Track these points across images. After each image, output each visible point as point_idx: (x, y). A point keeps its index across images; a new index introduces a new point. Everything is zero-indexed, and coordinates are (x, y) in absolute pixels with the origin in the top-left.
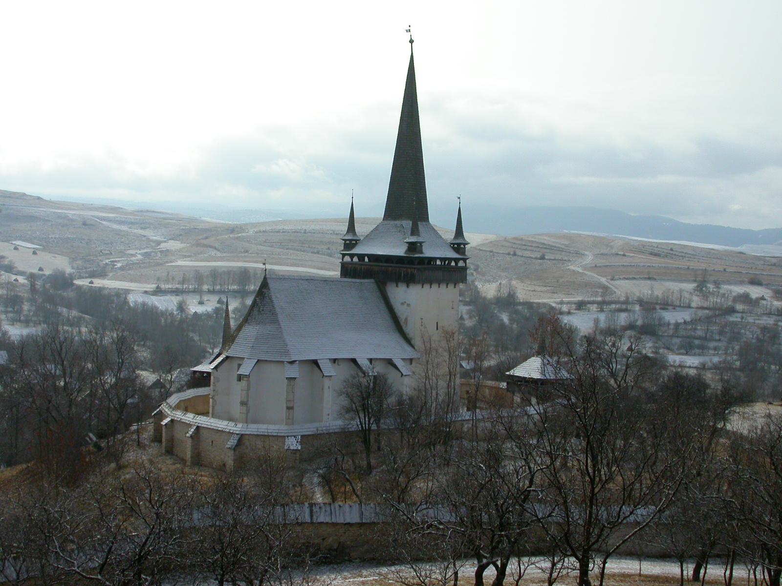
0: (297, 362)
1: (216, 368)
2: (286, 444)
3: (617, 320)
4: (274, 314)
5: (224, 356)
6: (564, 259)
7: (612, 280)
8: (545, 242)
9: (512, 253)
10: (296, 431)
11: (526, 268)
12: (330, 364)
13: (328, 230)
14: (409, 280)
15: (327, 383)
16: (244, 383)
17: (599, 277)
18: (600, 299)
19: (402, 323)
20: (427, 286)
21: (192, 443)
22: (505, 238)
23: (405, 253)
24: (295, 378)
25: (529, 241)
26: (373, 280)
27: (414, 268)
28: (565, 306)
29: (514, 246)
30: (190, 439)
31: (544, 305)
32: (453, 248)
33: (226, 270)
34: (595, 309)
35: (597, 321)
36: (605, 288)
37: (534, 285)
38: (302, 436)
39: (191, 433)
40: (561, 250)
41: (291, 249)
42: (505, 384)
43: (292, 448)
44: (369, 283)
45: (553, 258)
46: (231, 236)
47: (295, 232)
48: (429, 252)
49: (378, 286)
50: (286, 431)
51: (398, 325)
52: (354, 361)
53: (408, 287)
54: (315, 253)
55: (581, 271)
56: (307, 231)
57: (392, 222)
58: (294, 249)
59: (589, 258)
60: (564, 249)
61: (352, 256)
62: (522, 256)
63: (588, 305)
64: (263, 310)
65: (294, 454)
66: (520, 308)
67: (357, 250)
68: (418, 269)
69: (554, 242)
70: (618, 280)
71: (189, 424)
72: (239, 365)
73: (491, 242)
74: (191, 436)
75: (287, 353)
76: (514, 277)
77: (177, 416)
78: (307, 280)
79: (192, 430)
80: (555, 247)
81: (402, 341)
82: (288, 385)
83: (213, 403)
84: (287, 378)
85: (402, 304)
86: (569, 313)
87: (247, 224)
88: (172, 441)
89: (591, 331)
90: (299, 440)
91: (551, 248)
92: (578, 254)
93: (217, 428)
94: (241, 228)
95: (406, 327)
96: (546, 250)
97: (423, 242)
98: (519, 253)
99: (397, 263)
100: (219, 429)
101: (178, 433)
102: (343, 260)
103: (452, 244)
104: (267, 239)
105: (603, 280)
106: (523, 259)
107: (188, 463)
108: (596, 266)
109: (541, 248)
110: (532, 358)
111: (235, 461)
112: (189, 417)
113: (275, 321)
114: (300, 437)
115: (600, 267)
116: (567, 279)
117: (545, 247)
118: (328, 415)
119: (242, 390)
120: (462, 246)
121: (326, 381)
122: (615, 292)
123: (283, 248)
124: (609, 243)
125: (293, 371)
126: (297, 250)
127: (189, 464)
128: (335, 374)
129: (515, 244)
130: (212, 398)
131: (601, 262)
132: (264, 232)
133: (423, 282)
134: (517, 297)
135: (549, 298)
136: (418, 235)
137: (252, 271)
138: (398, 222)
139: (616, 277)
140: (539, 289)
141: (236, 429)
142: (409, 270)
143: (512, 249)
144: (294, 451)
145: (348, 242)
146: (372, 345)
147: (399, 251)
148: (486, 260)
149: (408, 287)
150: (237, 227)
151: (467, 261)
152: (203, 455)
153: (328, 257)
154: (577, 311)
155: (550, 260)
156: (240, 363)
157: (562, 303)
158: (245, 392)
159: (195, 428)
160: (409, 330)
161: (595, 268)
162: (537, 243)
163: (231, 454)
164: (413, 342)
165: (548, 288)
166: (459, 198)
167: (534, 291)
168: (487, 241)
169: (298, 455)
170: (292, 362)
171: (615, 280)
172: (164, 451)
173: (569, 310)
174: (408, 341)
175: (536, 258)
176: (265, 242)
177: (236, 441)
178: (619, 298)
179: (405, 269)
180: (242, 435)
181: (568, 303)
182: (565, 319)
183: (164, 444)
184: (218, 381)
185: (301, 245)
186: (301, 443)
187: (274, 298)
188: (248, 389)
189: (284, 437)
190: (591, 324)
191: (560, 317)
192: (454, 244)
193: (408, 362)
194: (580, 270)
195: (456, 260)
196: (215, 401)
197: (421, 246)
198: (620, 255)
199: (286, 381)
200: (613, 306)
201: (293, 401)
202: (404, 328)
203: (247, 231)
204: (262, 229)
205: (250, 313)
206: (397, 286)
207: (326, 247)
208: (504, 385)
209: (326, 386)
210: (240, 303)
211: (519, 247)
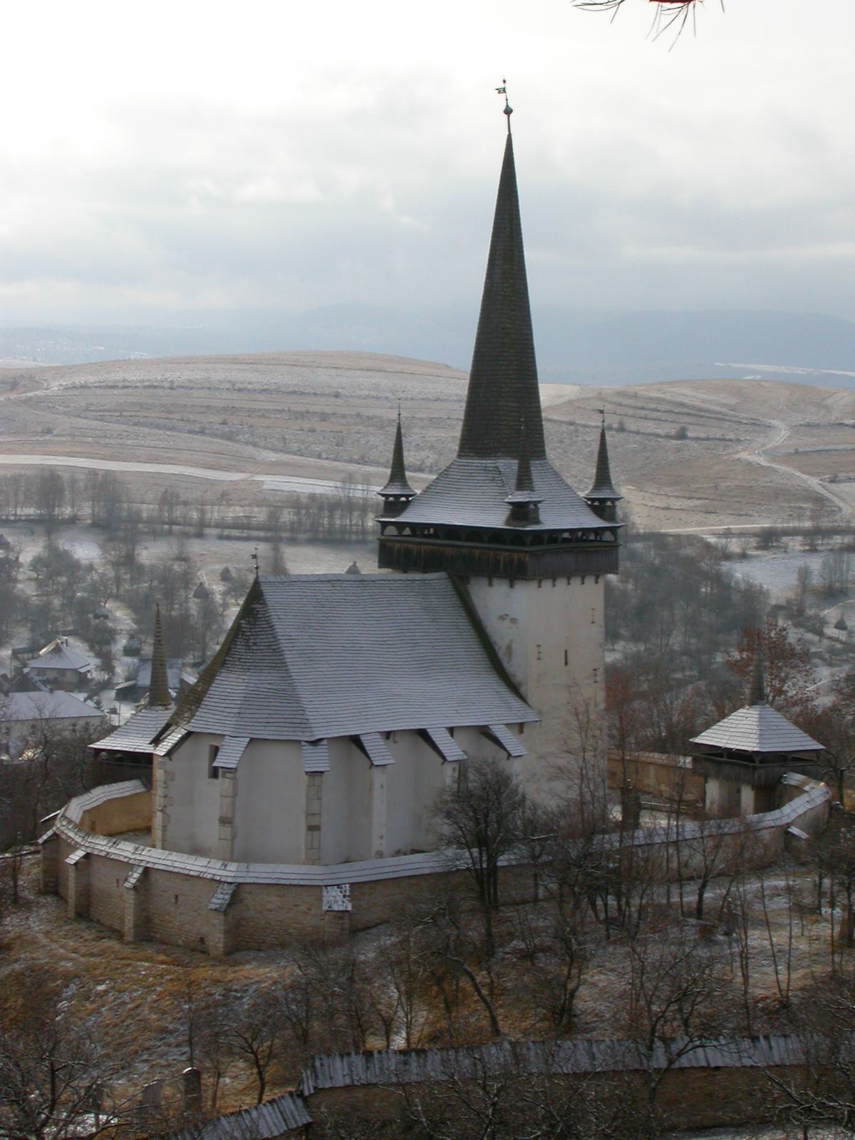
0: (325, 742)
1: (169, 754)
2: (325, 900)
3: (848, 570)
4: (277, 651)
5: (184, 732)
6: (727, 437)
7: (832, 481)
8: (686, 401)
9: (615, 426)
11: (648, 458)
12: (381, 741)
13: (221, 382)
14: (515, 573)
15: (379, 778)
16: (223, 784)
17: (805, 477)
18: (807, 524)
19: (501, 654)
20: (547, 584)
21: (134, 900)
22: (600, 393)
23: (507, 523)
24: (322, 772)
25: (651, 399)
26: (443, 574)
27: (522, 551)
28: (734, 540)
29: (620, 410)
30: (132, 892)
31: (691, 539)
32: (592, 507)
33: (9, 473)
34: (798, 548)
35: (804, 574)
36: (819, 500)
37: (666, 495)
38: (352, 885)
39: (133, 881)
40: (720, 418)
41: (145, 425)
42: (689, 759)
43: (335, 908)
44: (437, 579)
45: (702, 435)
46: (12, 397)
47: (150, 387)
48: (553, 519)
49: (456, 587)
50: (322, 877)
51: (495, 662)
52: (423, 734)
53: (512, 586)
54: (197, 433)
55: (764, 464)
56: (176, 384)
58: (151, 425)
59: (781, 436)
60: (727, 415)
61: (401, 526)
62: (638, 433)
63: (784, 539)
64: (255, 644)
65: (341, 918)
66: (639, 546)
67: (409, 516)
68: (532, 554)
69: (704, 401)
70: (845, 481)
71: (127, 863)
72: (215, 751)
73: (570, 402)
74: (135, 888)
75: (304, 724)
76: (623, 478)
77: (99, 847)
78: (329, 581)
79: (136, 875)
80: (708, 411)
81: (503, 689)
82: (309, 786)
83: (163, 820)
84: (307, 772)
86: (743, 556)
87: (43, 370)
88: (86, 894)
89: (791, 595)
90: (348, 893)
91: (699, 413)
92: (758, 426)
93: (187, 872)
94: (31, 378)
95: (508, 662)
96: (688, 419)
97: (540, 502)
98: (631, 425)
99: (489, 542)
100: (192, 873)
101: (102, 879)
102: (382, 534)
103: (589, 499)
104: (92, 404)
105: (814, 483)
106: (638, 438)
107: (129, 938)
108: (797, 452)
109: (679, 413)
110: (740, 710)
111: (226, 932)
112: (125, 850)
113: (279, 664)
114: (347, 886)
115: (806, 453)
116: (736, 482)
117: (686, 410)
118: (382, 837)
119: (222, 796)
120: (609, 503)
121: (377, 774)
122: (840, 509)
123: (126, 424)
124: (824, 400)
125: (319, 760)
126: (158, 427)
127: (131, 939)
128: (392, 761)
129: (620, 405)
130: (161, 811)
131: (808, 442)
132: (82, 387)
133: (540, 576)
134: (634, 524)
135: (700, 524)
136: (532, 489)
137: (66, 476)
138: (489, 463)
139: (842, 476)
140: (677, 504)
141: (225, 873)
142: (515, 556)
143: (617, 418)
144: (340, 914)
145: (391, 499)
146: (452, 701)
147: (495, 519)
148: (561, 442)
149: (512, 586)
150: (22, 377)
152: (157, 921)
153: (226, 442)
154: (759, 552)
155: (697, 439)
157: (728, 534)
158: (228, 800)
159: (140, 870)
160: (515, 667)
161: (795, 456)
162: (669, 402)
163: (218, 920)
164: (522, 690)
165: (698, 502)
167: (667, 508)
168: (561, 400)
169: (347, 921)
170: (315, 743)
171: (840, 482)
172: (72, 914)
173: (744, 549)
174: (514, 688)
175: (668, 437)
176: (87, 410)
177: (227, 897)
178: (848, 521)
179: (507, 554)
180: (240, 884)
181: (741, 534)
182: (739, 571)
183: (72, 900)
184: (173, 780)
185: (164, 415)
186: (352, 897)
187: (275, 621)
188: (235, 795)
190: (793, 580)
191: (725, 566)
192: (593, 500)
193: (516, 729)
194: (762, 461)
195: (597, 531)
196: (168, 815)
197: (537, 509)
198: (847, 425)
199: (306, 777)
200: (838, 540)
201: (319, 814)
202: (505, 664)
203: (45, 386)
204: (79, 379)
205: (230, 649)
206: (490, 584)
207: (217, 419)
208: (687, 762)
209: (377, 786)
210: (45, 547)
211: (631, 412)
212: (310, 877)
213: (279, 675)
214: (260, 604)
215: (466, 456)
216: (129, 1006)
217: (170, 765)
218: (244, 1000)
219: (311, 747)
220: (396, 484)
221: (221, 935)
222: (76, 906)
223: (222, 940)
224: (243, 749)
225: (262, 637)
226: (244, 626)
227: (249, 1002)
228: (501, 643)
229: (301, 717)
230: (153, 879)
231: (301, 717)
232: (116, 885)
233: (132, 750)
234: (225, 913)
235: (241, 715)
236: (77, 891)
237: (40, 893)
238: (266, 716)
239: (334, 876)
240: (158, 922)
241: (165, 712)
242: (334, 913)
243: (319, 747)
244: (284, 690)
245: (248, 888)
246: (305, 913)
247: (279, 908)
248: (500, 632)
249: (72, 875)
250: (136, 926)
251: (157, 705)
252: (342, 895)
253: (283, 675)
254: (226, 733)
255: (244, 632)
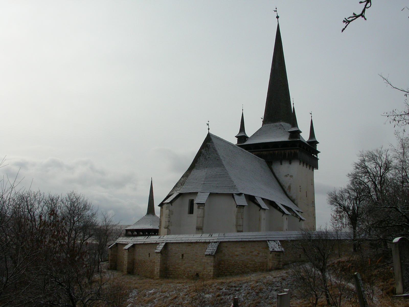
4: (218, 159)
10: (274, 236)
14: (290, 159)
19: (286, 190)
21: (161, 258)
23: (289, 139)
43: (276, 250)
53: (290, 164)
57: (272, 124)
64: (209, 158)
65: (279, 255)
74: (161, 252)
75: (234, 187)
85: (286, 176)
101: (141, 255)
111: (215, 267)
119: (198, 217)
138: (277, 124)
147: (285, 138)
149: (290, 164)
151: (318, 154)
156: (192, 198)
163: (210, 261)
164: (295, 202)
166: (311, 114)
179: (289, 151)
188: (203, 217)
189: (266, 241)
199: (236, 209)
201: (243, 225)
206: (281, 164)
212: (259, 237)
213: (221, 169)
214: (210, 143)
215: (268, 123)
216: (170, 298)
217: (171, 207)
218: (242, 291)
219: (238, 196)
220: (242, 133)
221: (212, 268)
222: (128, 268)
223: (212, 271)
224: (208, 196)
225: (212, 155)
226: (203, 152)
227: (244, 292)
228: (286, 186)
229: (233, 184)
230: (169, 249)
231: (233, 184)
232: (148, 256)
233: (141, 228)
234: (214, 256)
235: (205, 184)
236: (128, 262)
237: (108, 269)
238: (216, 184)
239: (271, 236)
240: (172, 269)
241: (153, 217)
242: (276, 253)
243: (241, 196)
244: (224, 174)
245: (225, 245)
246: (256, 256)
247: (242, 254)
248: (286, 181)
249: (126, 253)
250: (160, 271)
251: (150, 214)
252: (277, 245)
253: (222, 169)
254: (199, 191)
255: (203, 154)
